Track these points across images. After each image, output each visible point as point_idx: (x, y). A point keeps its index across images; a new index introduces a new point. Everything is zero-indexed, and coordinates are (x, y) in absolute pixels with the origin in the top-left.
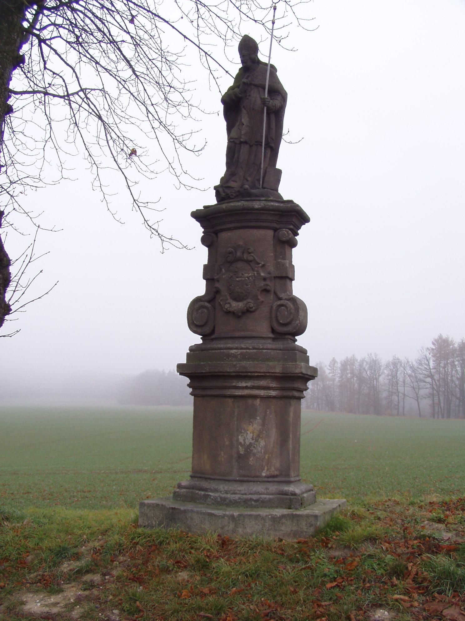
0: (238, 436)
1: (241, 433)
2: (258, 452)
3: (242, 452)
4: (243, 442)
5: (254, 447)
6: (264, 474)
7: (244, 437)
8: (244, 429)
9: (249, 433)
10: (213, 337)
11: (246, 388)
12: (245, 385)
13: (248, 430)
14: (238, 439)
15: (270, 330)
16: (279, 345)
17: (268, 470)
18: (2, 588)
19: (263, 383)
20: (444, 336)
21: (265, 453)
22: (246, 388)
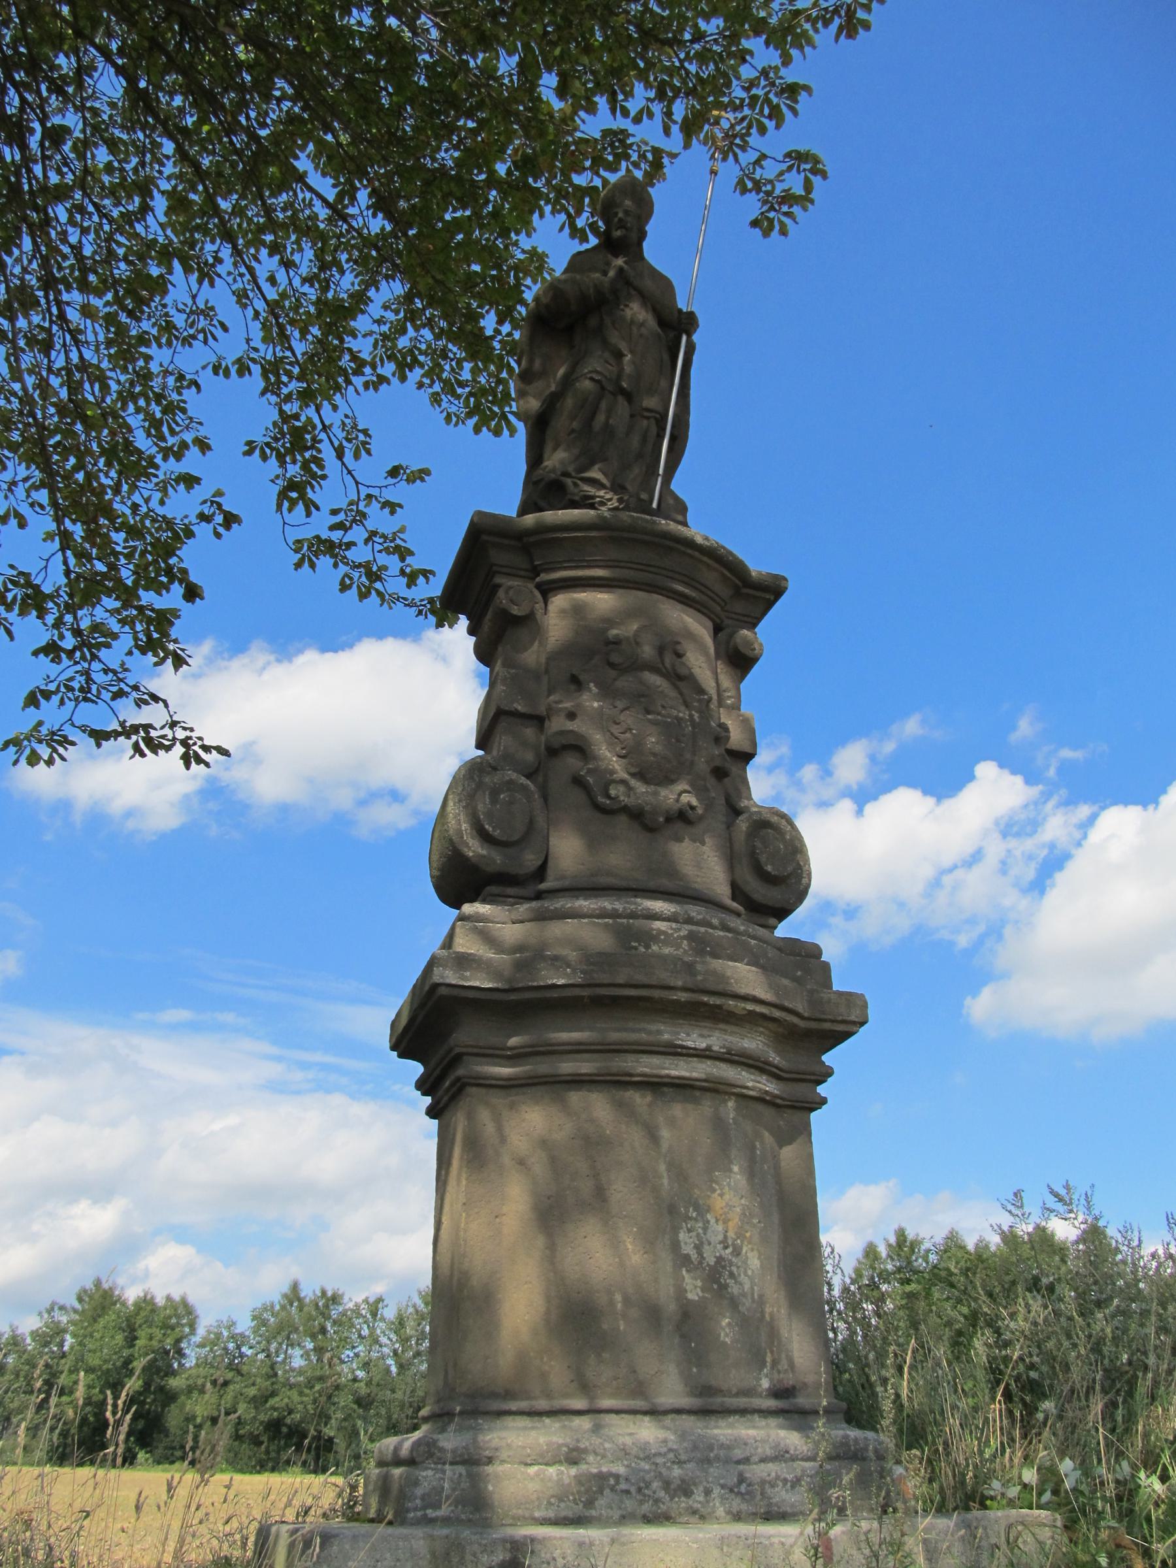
2: (744, 1295)
5: (732, 1275)
7: (698, 1235)
9: (713, 1221)
11: (705, 1055)
12: (704, 1045)
13: (708, 1211)
20: (177, 1297)
22: (705, 1055)
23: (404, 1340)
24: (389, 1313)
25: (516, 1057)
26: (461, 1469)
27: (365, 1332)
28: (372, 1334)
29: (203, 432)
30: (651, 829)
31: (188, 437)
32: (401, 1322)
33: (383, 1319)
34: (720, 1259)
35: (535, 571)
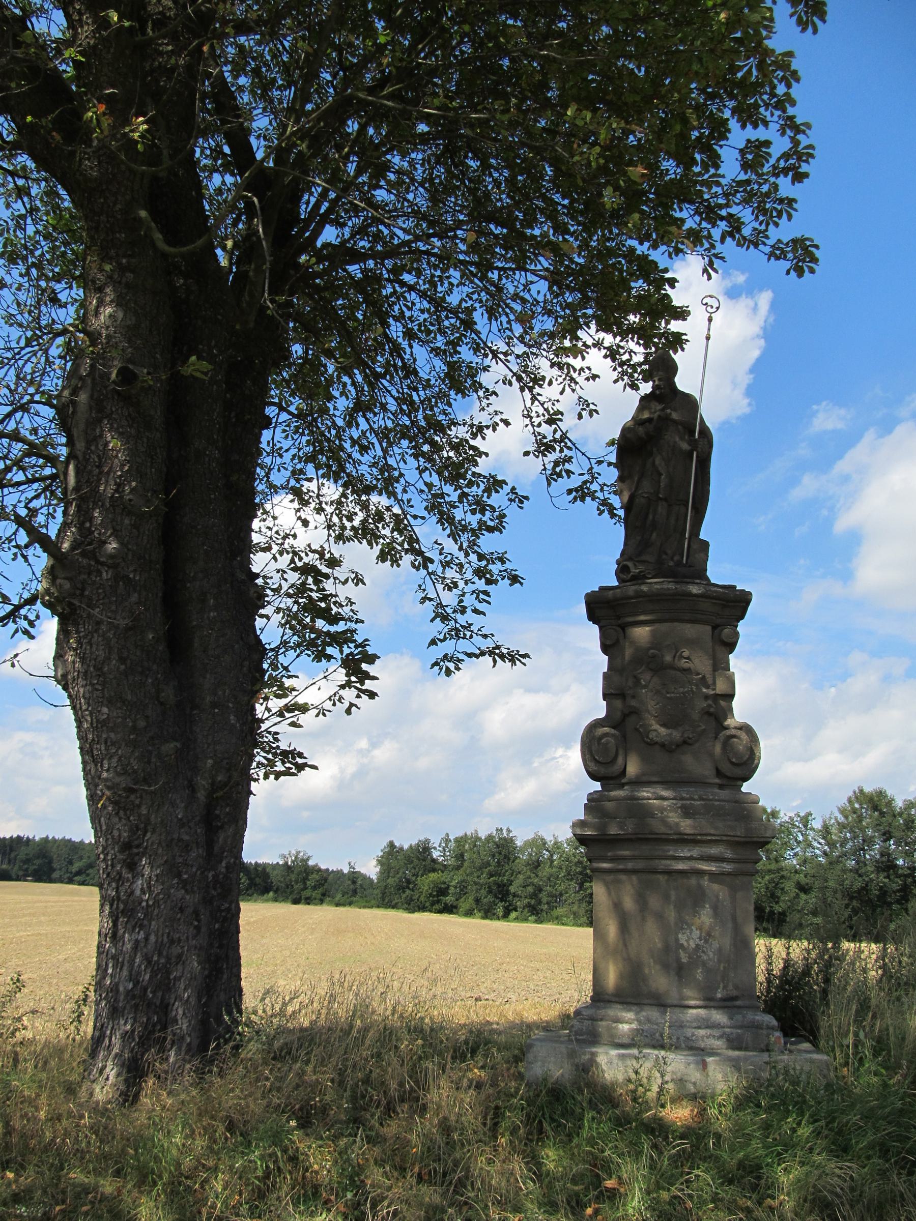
0: (677, 934)
1: (682, 929)
3: (684, 960)
4: (685, 944)
6: (719, 995)
8: (687, 924)
10: (623, 781)
11: (691, 858)
14: (677, 940)
15: (714, 772)
16: (724, 794)
17: (724, 988)
18: (383, 1218)
19: (714, 851)
21: (719, 961)
22: (691, 858)
23: (831, 844)
24: (817, 824)
25: (612, 860)
26: (590, 1022)
27: (800, 838)
28: (806, 840)
29: (504, 417)
30: (670, 751)
31: (497, 419)
32: (826, 831)
33: (812, 829)
34: (697, 945)
35: (619, 618)
